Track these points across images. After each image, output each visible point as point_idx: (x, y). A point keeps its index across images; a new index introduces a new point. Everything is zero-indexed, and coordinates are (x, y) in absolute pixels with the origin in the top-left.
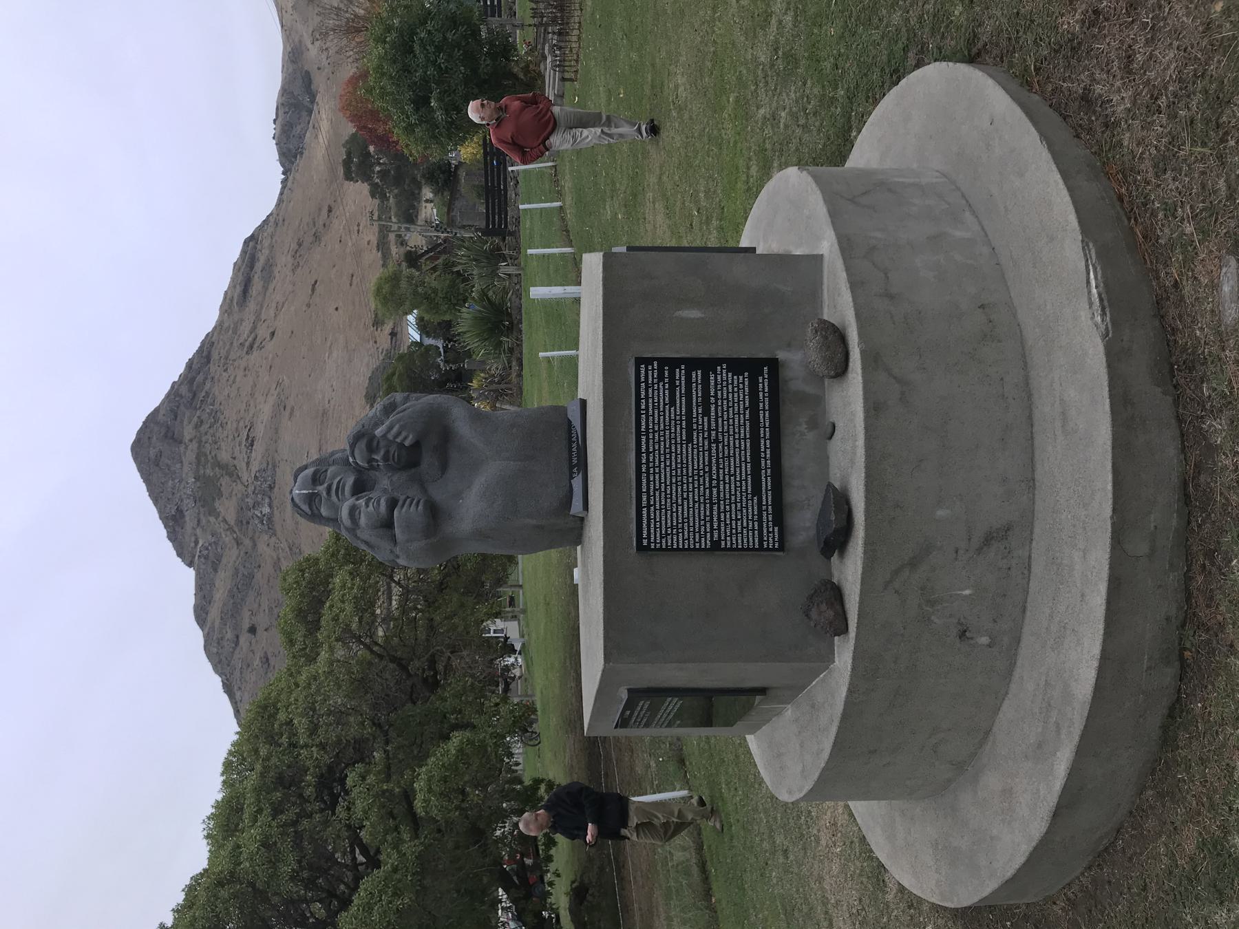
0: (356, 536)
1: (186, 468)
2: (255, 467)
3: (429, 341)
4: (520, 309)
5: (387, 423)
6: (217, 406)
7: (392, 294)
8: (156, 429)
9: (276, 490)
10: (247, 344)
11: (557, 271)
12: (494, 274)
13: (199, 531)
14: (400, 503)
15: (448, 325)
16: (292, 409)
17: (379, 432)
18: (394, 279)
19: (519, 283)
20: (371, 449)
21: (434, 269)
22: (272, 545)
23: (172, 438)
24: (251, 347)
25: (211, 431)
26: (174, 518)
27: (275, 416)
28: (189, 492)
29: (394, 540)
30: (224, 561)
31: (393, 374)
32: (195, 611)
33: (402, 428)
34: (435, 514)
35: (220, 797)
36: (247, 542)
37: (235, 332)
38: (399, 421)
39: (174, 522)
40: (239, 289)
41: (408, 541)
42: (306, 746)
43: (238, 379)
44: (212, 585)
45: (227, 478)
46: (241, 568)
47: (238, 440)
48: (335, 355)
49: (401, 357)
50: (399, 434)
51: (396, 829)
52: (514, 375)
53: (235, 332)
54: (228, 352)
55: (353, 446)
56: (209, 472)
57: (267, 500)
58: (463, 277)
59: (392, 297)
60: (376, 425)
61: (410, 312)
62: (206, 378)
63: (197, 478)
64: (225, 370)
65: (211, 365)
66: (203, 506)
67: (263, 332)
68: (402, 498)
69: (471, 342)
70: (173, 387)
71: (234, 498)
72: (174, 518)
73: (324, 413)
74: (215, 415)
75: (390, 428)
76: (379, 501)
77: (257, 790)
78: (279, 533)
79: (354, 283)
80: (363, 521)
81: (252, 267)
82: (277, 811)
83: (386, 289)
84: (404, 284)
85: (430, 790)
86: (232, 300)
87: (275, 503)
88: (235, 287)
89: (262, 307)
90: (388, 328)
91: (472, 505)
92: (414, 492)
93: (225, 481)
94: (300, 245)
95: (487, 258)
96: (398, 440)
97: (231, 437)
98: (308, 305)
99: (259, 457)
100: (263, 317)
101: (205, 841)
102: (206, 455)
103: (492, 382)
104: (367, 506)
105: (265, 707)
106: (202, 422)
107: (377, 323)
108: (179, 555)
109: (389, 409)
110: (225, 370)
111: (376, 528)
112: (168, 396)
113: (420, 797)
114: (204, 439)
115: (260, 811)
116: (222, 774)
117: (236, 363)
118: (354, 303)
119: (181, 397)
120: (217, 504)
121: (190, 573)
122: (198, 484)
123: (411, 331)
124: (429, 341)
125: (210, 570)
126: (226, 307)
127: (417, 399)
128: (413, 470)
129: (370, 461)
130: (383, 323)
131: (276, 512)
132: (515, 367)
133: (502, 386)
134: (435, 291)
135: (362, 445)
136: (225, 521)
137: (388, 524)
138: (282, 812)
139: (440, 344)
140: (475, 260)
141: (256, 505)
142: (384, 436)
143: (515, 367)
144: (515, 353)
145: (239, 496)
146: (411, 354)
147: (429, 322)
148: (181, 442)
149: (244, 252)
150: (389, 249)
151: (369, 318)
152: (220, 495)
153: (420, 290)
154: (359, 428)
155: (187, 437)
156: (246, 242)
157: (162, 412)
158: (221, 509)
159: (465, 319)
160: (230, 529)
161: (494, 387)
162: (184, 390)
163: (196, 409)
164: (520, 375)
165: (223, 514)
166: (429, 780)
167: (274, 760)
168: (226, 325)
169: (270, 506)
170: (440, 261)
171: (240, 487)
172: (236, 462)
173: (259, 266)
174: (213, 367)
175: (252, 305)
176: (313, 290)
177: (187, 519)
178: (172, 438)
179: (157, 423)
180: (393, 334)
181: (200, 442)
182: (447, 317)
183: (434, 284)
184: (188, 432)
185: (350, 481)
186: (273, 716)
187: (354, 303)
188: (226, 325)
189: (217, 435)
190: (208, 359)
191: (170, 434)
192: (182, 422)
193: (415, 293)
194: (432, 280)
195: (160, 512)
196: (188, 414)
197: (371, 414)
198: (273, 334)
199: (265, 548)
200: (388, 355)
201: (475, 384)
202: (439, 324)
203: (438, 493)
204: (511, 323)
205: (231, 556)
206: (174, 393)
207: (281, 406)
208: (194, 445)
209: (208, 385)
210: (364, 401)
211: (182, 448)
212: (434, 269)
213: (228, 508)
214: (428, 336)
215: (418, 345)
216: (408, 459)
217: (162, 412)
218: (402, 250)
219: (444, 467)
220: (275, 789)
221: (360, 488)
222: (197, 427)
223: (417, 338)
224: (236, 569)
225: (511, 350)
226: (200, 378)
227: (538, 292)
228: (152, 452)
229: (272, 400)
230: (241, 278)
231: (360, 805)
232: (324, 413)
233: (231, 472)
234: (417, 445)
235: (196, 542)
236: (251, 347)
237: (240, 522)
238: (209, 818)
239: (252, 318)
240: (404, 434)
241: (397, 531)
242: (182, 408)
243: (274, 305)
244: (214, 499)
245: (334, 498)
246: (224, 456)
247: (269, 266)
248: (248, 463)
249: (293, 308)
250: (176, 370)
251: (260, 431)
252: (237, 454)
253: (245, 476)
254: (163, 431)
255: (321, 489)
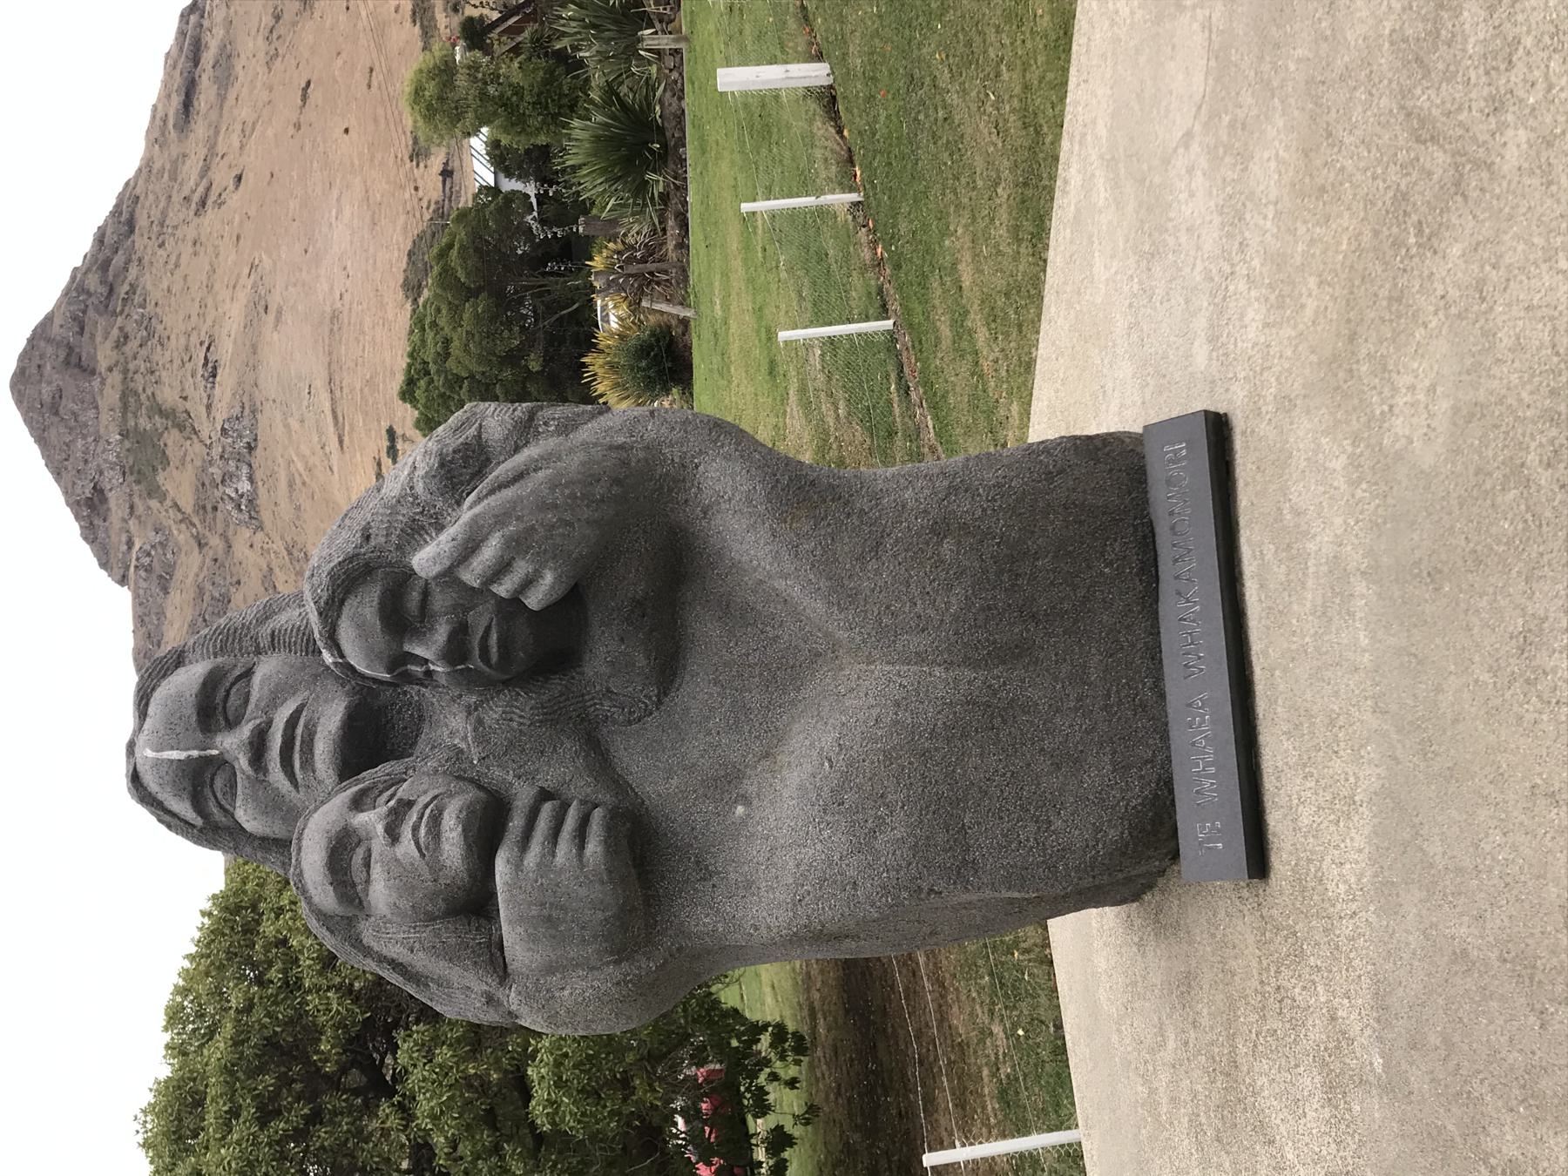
0: (357, 943)
1: (105, 417)
2: (220, 415)
3: (509, 185)
4: (680, 116)
5: (454, 531)
6: (150, 307)
7: (441, 99)
8: (50, 350)
9: (259, 452)
10: (196, 198)
11: (759, 37)
12: (631, 51)
13: (133, 525)
14: (516, 823)
15: (544, 153)
16: (279, 312)
17: (426, 559)
18: (445, 71)
19: (678, 67)
20: (400, 618)
21: (516, 50)
22: (257, 546)
23: (79, 365)
24: (203, 203)
25: (143, 352)
26: (90, 504)
27: (250, 324)
28: (112, 458)
29: (495, 961)
30: (178, 575)
31: (450, 246)
32: (135, 660)
33: (516, 546)
34: (648, 862)
35: (165, 1072)
36: (215, 541)
37: (173, 177)
38: (501, 519)
39: (90, 509)
40: (177, 100)
41: (550, 969)
42: (317, 989)
43: (183, 260)
44: (161, 614)
45: (175, 432)
46: (208, 586)
47: (189, 366)
48: (347, 211)
49: (463, 215)
50: (501, 568)
51: (496, 1149)
52: (671, 245)
53: (173, 177)
54: (164, 214)
55: (331, 610)
56: (144, 423)
57: (245, 470)
58: (569, 62)
59: (443, 104)
60: (415, 532)
61: (476, 132)
62: (128, 261)
63: (124, 435)
64: (161, 245)
65: (136, 236)
66: (138, 482)
67: (222, 176)
68: (523, 796)
69: (591, 185)
70: (73, 278)
71: (189, 467)
72: (90, 504)
73: (335, 316)
74: (147, 323)
75: (469, 548)
76: (436, 820)
77: (228, 1070)
78: (268, 524)
79: (375, 83)
80: (380, 893)
81: (196, 60)
82: (266, 1114)
83: (431, 89)
84: (461, 81)
85: (560, 1084)
86: (165, 122)
87: (258, 475)
88: (169, 96)
89: (217, 133)
90: (436, 162)
91: (794, 824)
92: (562, 768)
93: (172, 438)
94: (278, 18)
95: (616, 22)
96: (503, 589)
97: (177, 362)
98: (298, 126)
99: (228, 394)
100: (221, 149)
101: (141, 1152)
102: (136, 393)
103: (630, 260)
104: (393, 834)
105: (237, 909)
106: (126, 337)
107: (418, 154)
108: (104, 565)
109: (461, 471)
110: (161, 245)
111: (431, 918)
112: (66, 292)
113: (540, 1093)
114: (131, 366)
115: (235, 1113)
116: (166, 1029)
117: (179, 233)
118: (375, 120)
119: (89, 294)
120: (160, 478)
121: (124, 596)
122: (127, 444)
123: (477, 167)
124: (509, 185)
125: (156, 590)
126: (156, 134)
127: (566, 428)
128: (556, 685)
129: (398, 662)
130: (427, 155)
131: (262, 491)
132: (673, 230)
133: (650, 266)
134: (518, 91)
135: (364, 607)
136: (176, 505)
137: (472, 904)
138: (277, 1113)
139: (531, 189)
140: (594, 26)
141: (227, 478)
142: (449, 576)
143: (673, 230)
144: (673, 206)
145: (198, 463)
146: (479, 209)
147: (509, 149)
148: (93, 372)
149: (182, 33)
150: (433, 18)
151: (403, 146)
152: (165, 461)
153: (491, 90)
154: (347, 541)
155: (103, 365)
156: (185, 16)
157: (57, 321)
158: (168, 486)
159: (579, 139)
160: (186, 520)
161: (634, 268)
162: (93, 282)
163: (114, 314)
164: (683, 246)
165: (172, 493)
166: (558, 1064)
167: (258, 1013)
168: (157, 166)
169: (251, 479)
170: (526, 34)
171: (198, 447)
172: (188, 405)
173: (208, 58)
174: (139, 241)
175: (200, 129)
176: (304, 98)
177: (112, 503)
178: (79, 365)
179: (49, 340)
180: (447, 173)
181: (125, 371)
182: (542, 140)
183: (517, 77)
184: (104, 355)
185: (331, 717)
186: (250, 929)
187: (375, 120)
188: (157, 166)
189: (155, 358)
190: (131, 225)
191: (74, 360)
192: (93, 336)
193: (483, 95)
194: (513, 71)
195: (66, 493)
196: (102, 322)
197: (392, 488)
198: (239, 178)
199: (247, 552)
200: (440, 213)
201: (598, 263)
202: (528, 152)
203: (655, 776)
204: (665, 146)
205: (190, 566)
206: (77, 289)
207: (260, 306)
208: (115, 378)
209: (133, 271)
210: (401, 294)
211: (96, 383)
212: (516, 50)
213: (179, 485)
214: (509, 175)
215: (494, 191)
216: (536, 653)
217: (57, 321)
218: (456, 20)
219: (668, 667)
220: (261, 1070)
221: (373, 739)
222: (118, 346)
223: (490, 179)
224: (201, 591)
225: (665, 198)
226: (118, 260)
227: (734, 79)
228: (46, 391)
229: (243, 296)
230: (178, 80)
231: (424, 1105)
232: (335, 316)
233: (182, 422)
234: (572, 601)
235: (130, 544)
236: (203, 203)
237: (201, 508)
238: (144, 1111)
239: (203, 152)
240: (522, 568)
241: (510, 933)
242: (91, 313)
243: (239, 127)
244: (154, 469)
245: (276, 775)
246: (168, 396)
247: (226, 57)
248: (209, 407)
249: (270, 132)
250: (76, 248)
251: (225, 351)
252: (189, 391)
253: (205, 431)
254: (62, 355)
255: (233, 743)
